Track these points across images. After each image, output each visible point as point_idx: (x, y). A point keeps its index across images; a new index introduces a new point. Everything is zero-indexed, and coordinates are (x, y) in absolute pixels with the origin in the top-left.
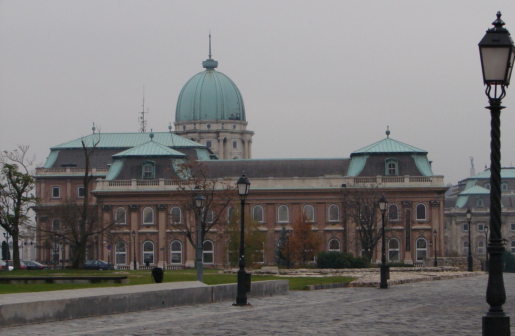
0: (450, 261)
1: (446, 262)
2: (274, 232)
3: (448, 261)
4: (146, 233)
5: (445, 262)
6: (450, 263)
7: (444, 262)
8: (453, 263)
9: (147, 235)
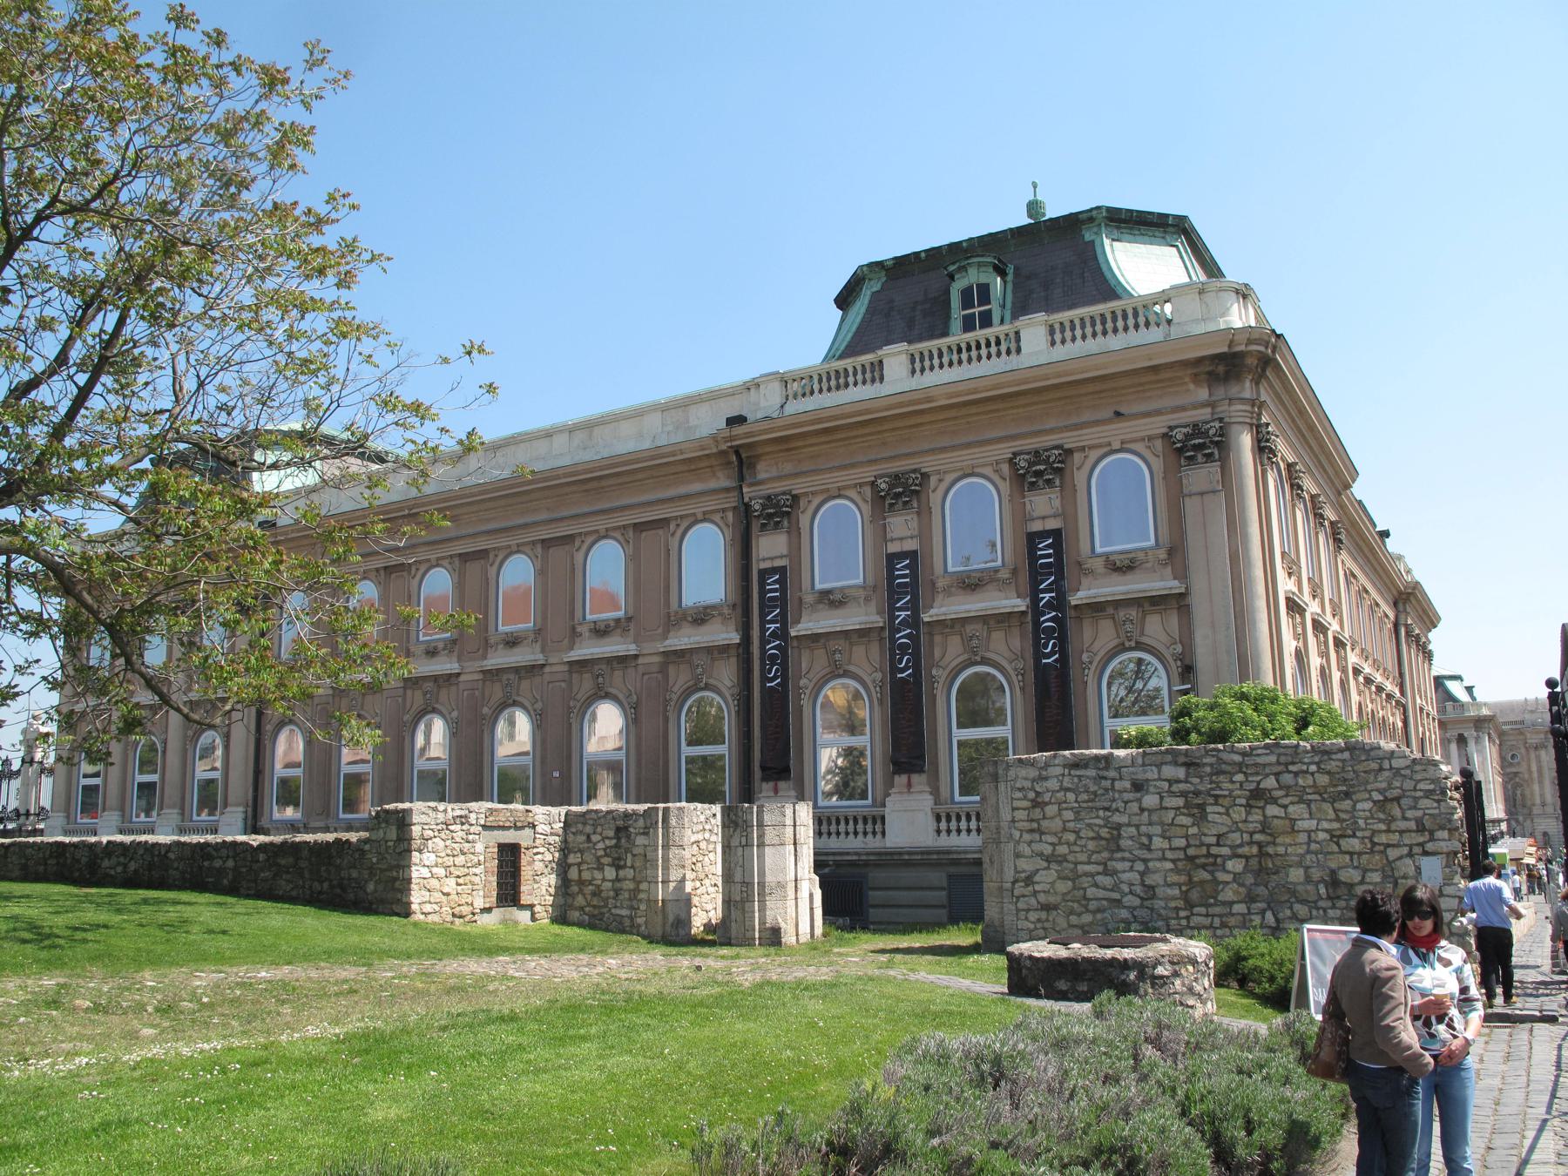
0: (1169, 771)
1: (1138, 786)
2: (480, 676)
3: (1152, 773)
4: (964, 621)
5: (1127, 785)
6: (1171, 793)
7: (1118, 785)
8: (1197, 793)
9: (970, 629)
